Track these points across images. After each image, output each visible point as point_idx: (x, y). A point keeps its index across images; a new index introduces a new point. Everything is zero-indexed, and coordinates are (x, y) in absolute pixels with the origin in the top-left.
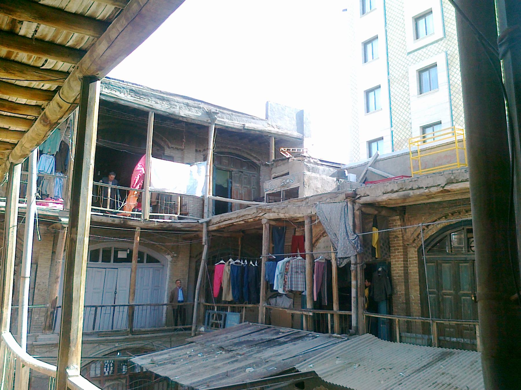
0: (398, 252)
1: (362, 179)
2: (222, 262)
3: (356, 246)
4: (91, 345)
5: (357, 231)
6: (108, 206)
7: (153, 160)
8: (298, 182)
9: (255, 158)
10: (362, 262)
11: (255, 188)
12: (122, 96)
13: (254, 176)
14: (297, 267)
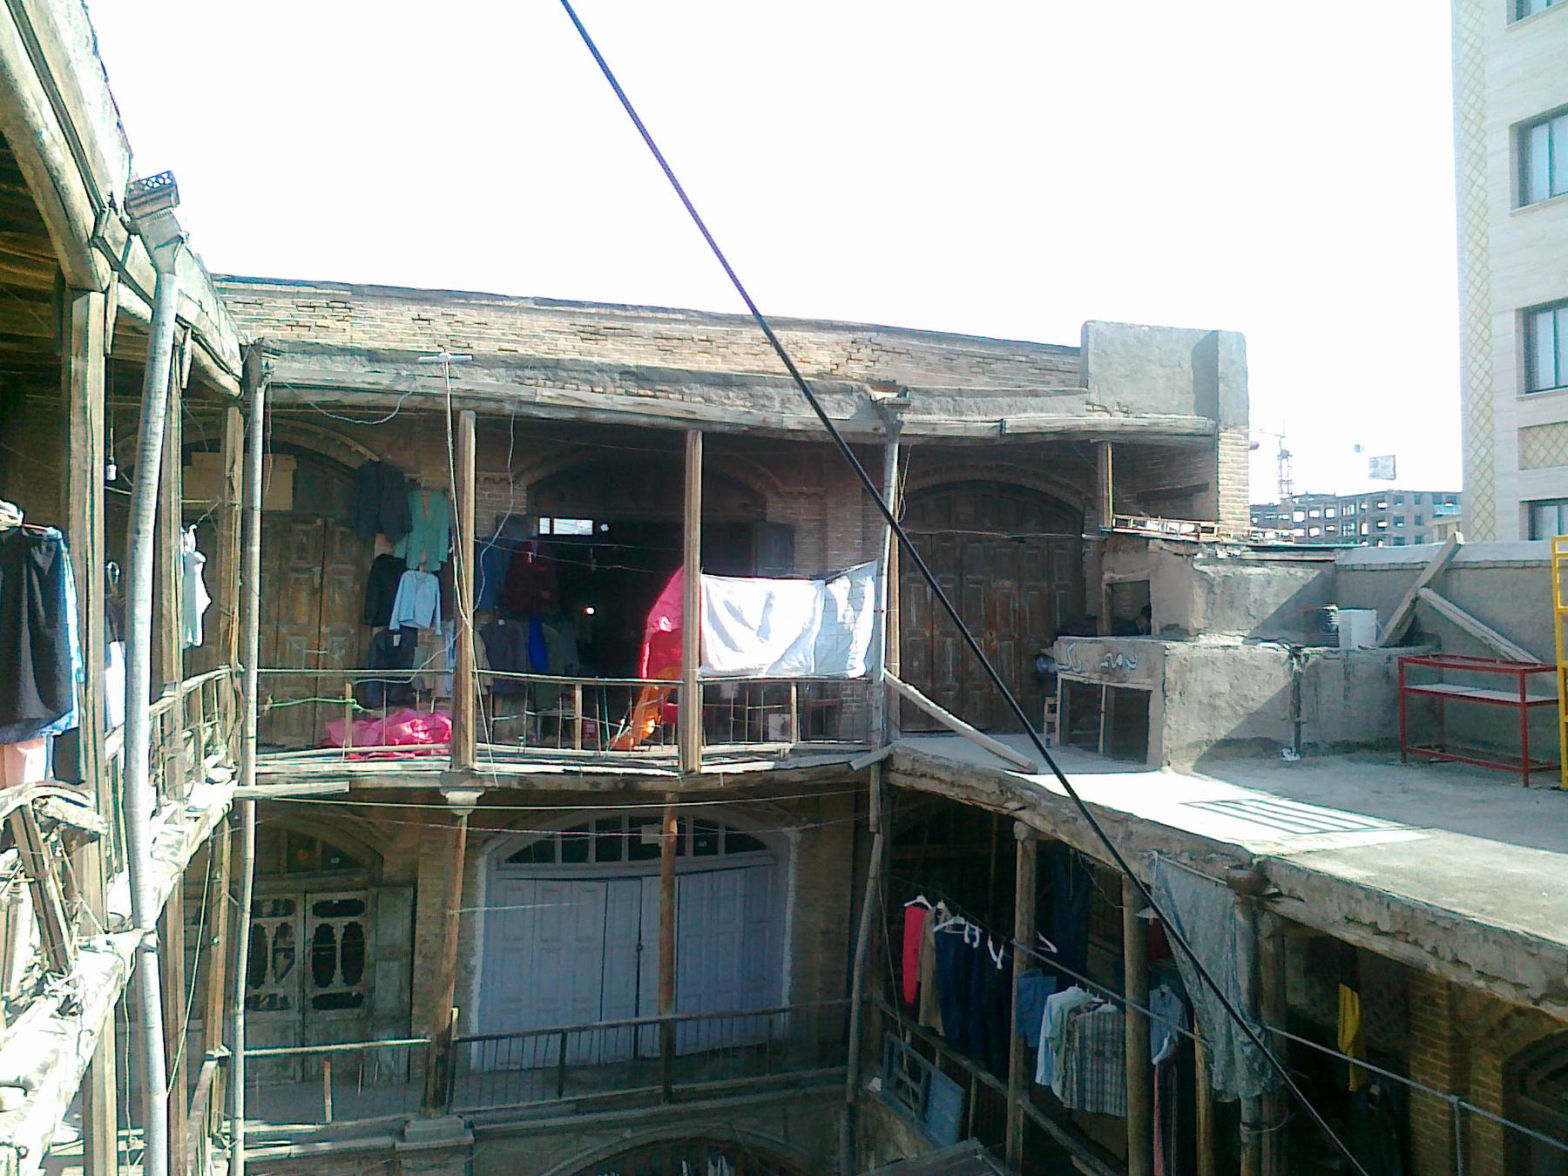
0: (1435, 1056)
1: (1398, 629)
2: (921, 899)
3: (1256, 1066)
4: (553, 1139)
5: (1265, 1013)
6: (578, 743)
7: (706, 581)
8: (1150, 676)
9: (1068, 487)
10: (1278, 1121)
11: (1066, 587)
12: (598, 399)
13: (1063, 548)
14: (1100, 1036)
